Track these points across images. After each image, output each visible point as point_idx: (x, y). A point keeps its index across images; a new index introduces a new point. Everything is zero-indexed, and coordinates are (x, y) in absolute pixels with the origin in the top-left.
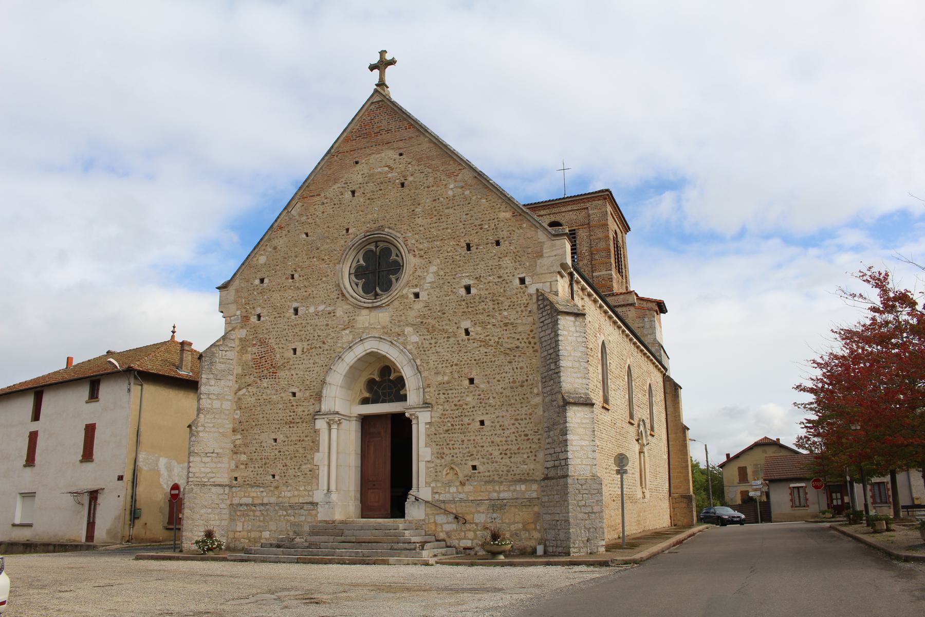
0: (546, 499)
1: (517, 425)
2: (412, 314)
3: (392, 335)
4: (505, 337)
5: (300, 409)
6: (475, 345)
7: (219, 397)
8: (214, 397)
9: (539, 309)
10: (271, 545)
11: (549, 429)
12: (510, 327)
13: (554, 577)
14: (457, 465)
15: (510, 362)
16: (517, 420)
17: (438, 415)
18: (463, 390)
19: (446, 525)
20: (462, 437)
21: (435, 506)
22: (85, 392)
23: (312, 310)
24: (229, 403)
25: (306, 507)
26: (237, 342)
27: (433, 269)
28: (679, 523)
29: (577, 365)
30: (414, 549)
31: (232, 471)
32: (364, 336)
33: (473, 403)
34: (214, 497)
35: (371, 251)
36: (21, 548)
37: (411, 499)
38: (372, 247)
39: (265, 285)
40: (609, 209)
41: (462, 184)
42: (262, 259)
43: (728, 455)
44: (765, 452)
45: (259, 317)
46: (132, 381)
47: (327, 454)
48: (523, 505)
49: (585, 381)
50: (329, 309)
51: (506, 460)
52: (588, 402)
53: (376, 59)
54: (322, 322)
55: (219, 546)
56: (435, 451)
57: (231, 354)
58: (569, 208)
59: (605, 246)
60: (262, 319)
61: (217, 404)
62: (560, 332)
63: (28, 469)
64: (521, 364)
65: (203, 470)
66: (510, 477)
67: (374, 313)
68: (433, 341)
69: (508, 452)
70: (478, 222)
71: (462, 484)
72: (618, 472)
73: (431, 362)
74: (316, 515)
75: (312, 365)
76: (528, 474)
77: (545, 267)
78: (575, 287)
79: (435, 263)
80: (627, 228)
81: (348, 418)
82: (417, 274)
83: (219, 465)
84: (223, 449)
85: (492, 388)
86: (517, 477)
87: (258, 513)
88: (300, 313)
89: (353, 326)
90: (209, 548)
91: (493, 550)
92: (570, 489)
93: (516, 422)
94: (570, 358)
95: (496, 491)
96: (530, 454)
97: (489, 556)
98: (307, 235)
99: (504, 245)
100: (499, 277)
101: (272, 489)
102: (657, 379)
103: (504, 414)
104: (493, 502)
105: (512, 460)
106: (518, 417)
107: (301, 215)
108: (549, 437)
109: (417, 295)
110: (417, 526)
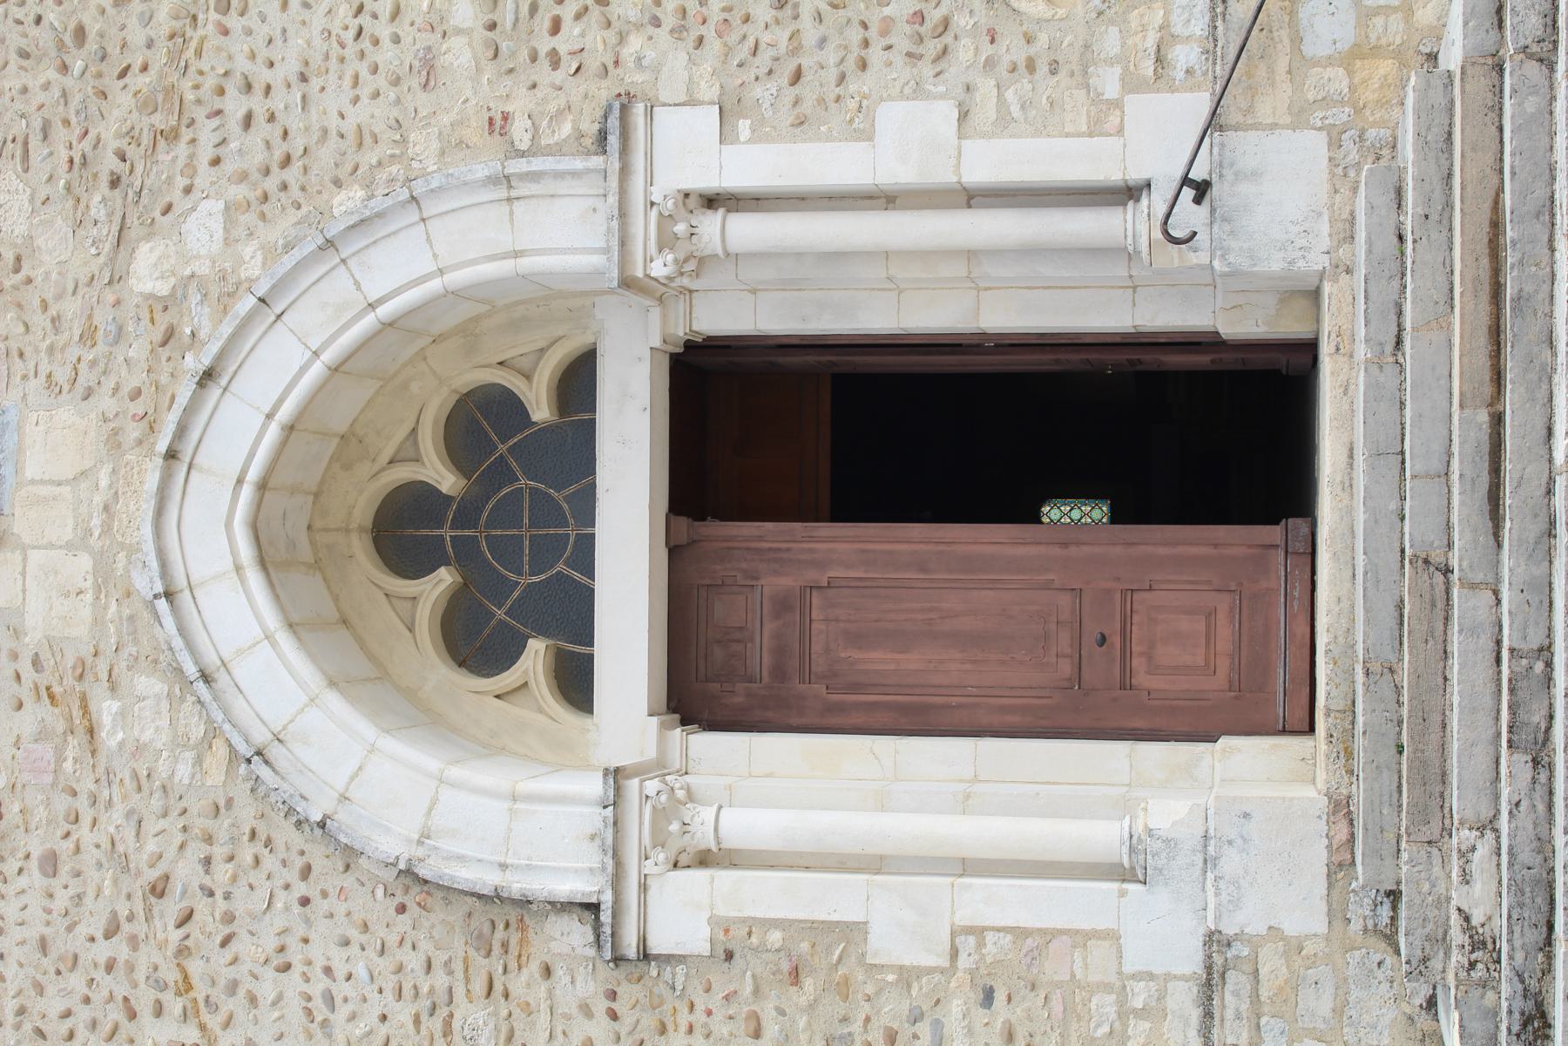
17: (677, 59)
68: (236, 106)
73: (356, 116)
74: (1294, 947)
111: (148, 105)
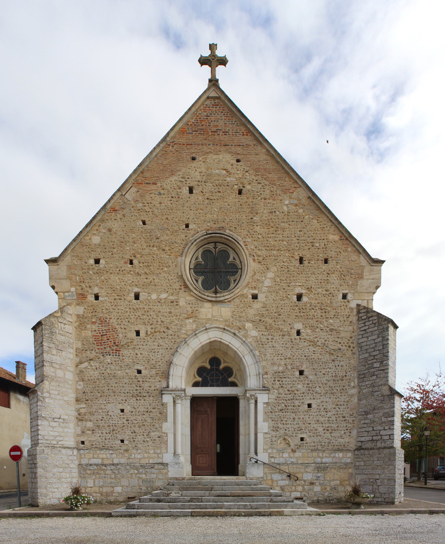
1: (337, 409)
2: (251, 312)
5: (146, 385)
6: (306, 344)
7: (62, 366)
8: (57, 366)
14: (290, 436)
15: (333, 361)
16: (337, 405)
18: (295, 379)
20: (293, 415)
21: (273, 467)
25: (156, 466)
27: (270, 275)
35: (210, 251)
38: (211, 246)
41: (296, 202)
48: (340, 468)
50: (171, 298)
54: (165, 309)
56: (272, 425)
60: (100, 298)
61: (60, 373)
64: (342, 363)
65: (51, 433)
66: (330, 447)
67: (216, 307)
68: (270, 337)
69: (329, 429)
71: (293, 451)
73: (268, 354)
74: (167, 474)
77: (364, 288)
79: (272, 270)
83: (66, 430)
84: (69, 415)
85: (319, 380)
86: (336, 447)
87: (109, 472)
88: (141, 298)
93: (337, 407)
95: (320, 457)
96: (346, 431)
98: (144, 223)
100: (326, 290)
101: (122, 451)
103: (327, 400)
104: (318, 465)
105: (333, 435)
106: (338, 403)
109: (255, 297)
111: (270, 325)
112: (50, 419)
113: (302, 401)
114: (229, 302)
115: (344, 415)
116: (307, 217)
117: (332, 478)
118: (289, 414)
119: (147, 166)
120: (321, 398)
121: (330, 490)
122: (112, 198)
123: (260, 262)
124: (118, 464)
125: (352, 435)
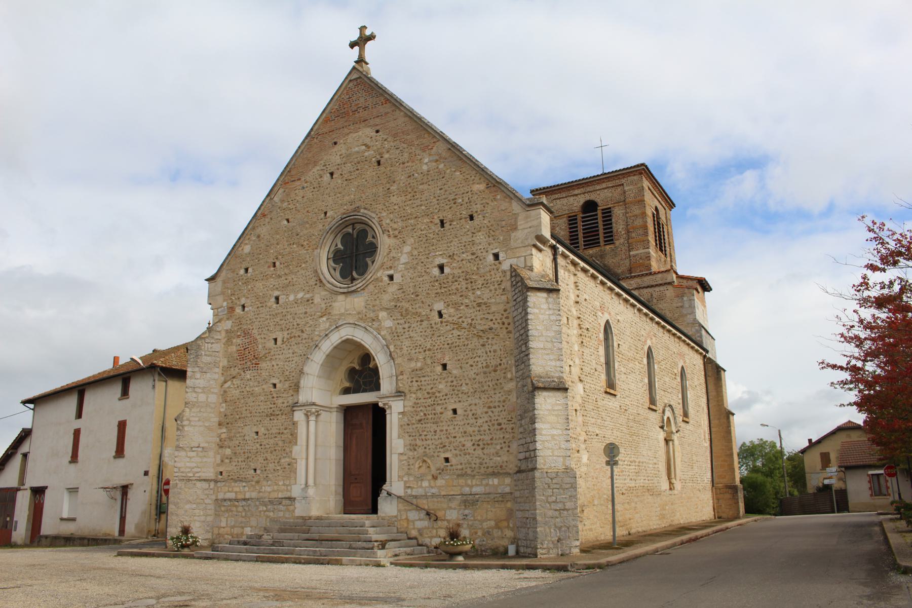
0: (517, 494)
1: (490, 413)
2: (386, 297)
3: (367, 320)
4: (478, 318)
5: (280, 400)
7: (205, 390)
8: (200, 391)
9: (512, 286)
10: (239, 543)
11: (522, 417)
12: (484, 307)
13: (534, 579)
14: (430, 457)
15: (483, 345)
16: (489, 407)
18: (436, 377)
19: (417, 522)
20: (434, 427)
21: (406, 501)
22: (117, 389)
23: (292, 298)
24: (215, 396)
25: (284, 502)
26: (224, 334)
27: (407, 249)
28: (724, 515)
29: (549, 345)
30: (372, 548)
31: (218, 465)
32: (340, 323)
33: (446, 391)
34: (199, 492)
35: (348, 234)
36: (63, 542)
37: (383, 494)
38: (350, 230)
39: (249, 275)
40: (646, 184)
41: (437, 157)
42: (247, 249)
43: (810, 441)
44: (849, 436)
45: (244, 307)
46: (157, 378)
47: (305, 447)
49: (558, 363)
50: (308, 296)
51: (479, 452)
52: (561, 386)
53: (355, 36)
54: (301, 310)
55: (195, 542)
56: (408, 442)
57: (217, 347)
58: (604, 185)
59: (641, 223)
60: (246, 309)
61: (202, 398)
62: (529, 310)
63: (73, 465)
64: (495, 347)
65: (188, 464)
66: (482, 470)
67: (350, 299)
68: (406, 326)
69: (481, 443)
70: (452, 197)
71: (435, 478)
72: (608, 463)
73: (405, 348)
74: (294, 511)
75: (291, 355)
76: (501, 467)
77: (519, 241)
78: (560, 260)
79: (409, 242)
80: (671, 205)
81: (328, 409)
82: (391, 255)
84: (208, 443)
86: (490, 470)
87: (240, 509)
88: (281, 301)
89: (329, 313)
90: (185, 546)
91: (448, 553)
92: (538, 483)
93: (489, 410)
94: (541, 339)
95: (468, 486)
96: (503, 445)
97: (447, 557)
98: (288, 221)
99: (477, 221)
100: (473, 254)
102: (694, 362)
103: (477, 401)
104: (465, 498)
105: (485, 451)
106: (491, 405)
107: (282, 201)
108: (521, 426)
109: (391, 278)
110: (390, 523)
111: (406, 310)
112: (188, 449)
113: (444, 406)
114: (363, 289)
115: (500, 421)
116: (448, 171)
117: (485, 517)
118: (428, 425)
119: (294, 164)
120: (469, 399)
121: (483, 535)
122: (261, 205)
123: (396, 237)
124: (248, 499)
125: (511, 451)
